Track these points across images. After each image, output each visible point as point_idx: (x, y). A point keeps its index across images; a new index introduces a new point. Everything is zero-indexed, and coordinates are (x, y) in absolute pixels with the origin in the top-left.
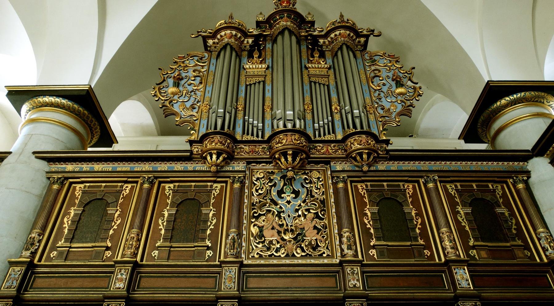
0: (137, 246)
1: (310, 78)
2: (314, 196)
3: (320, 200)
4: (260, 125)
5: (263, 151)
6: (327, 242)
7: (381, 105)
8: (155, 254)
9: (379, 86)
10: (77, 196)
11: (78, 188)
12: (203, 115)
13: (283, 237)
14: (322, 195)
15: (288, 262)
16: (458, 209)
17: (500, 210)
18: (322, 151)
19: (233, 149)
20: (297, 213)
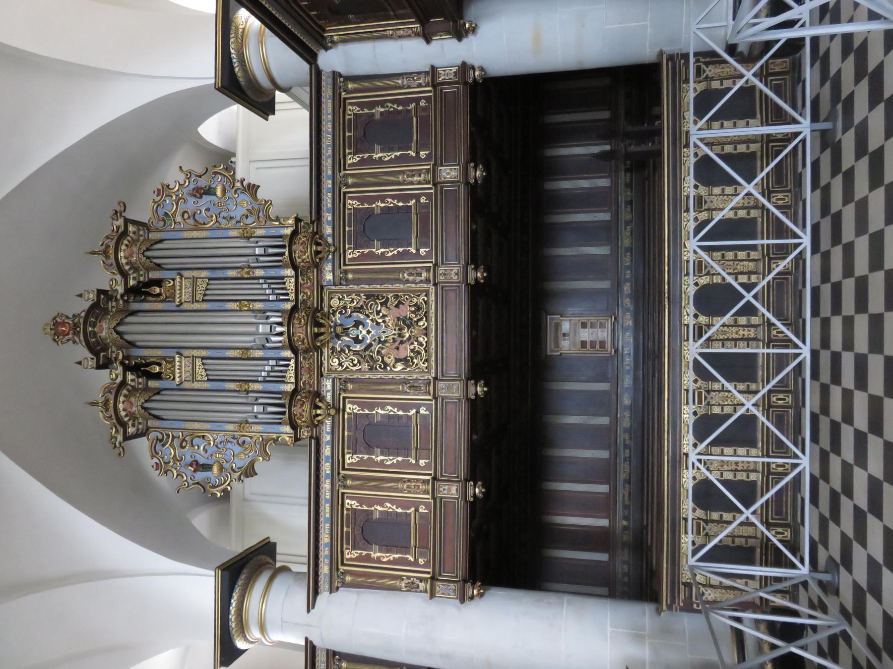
2: (362, 306)
3: (366, 299)
4: (272, 362)
5: (309, 359)
6: (412, 296)
9: (212, 216)
11: (348, 557)
15: (433, 334)
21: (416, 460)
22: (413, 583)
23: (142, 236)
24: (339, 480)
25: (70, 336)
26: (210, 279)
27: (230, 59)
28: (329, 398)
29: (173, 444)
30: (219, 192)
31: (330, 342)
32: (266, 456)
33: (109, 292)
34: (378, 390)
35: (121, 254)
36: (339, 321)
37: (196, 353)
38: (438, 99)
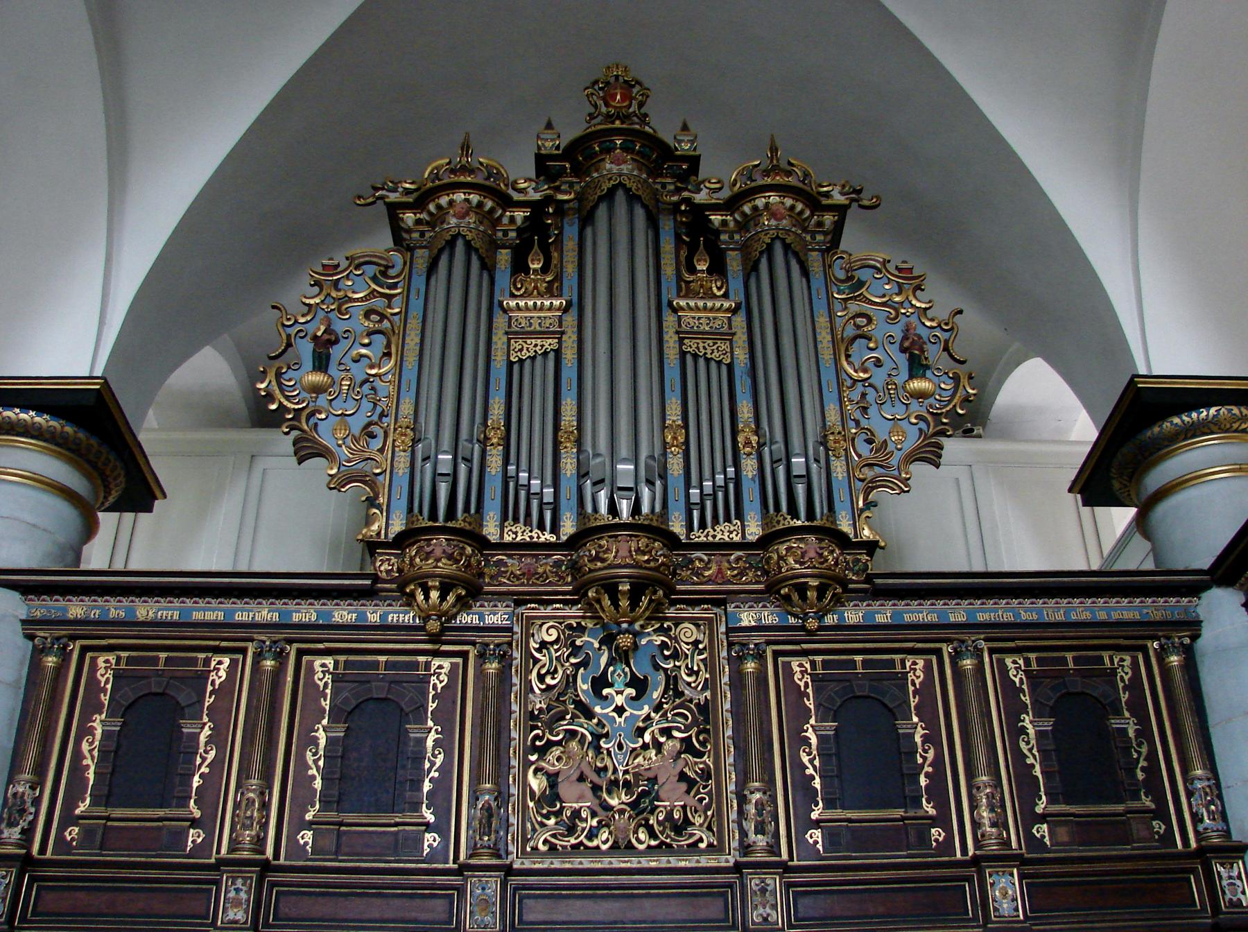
0: (264, 820)
1: (681, 340)
2: (682, 694)
3: (698, 705)
4: (549, 491)
6: (709, 813)
7: (867, 429)
8: (306, 840)
9: (865, 371)
10: (102, 685)
11: (101, 662)
12: (396, 459)
13: (605, 800)
14: (701, 690)
15: (617, 863)
16: (1023, 721)
17: (1118, 721)
18: (707, 573)
19: (480, 569)
20: (640, 740)
21: (311, 823)
22: (22, 811)
23: (813, 238)
24: (275, 642)
25: (604, 110)
26: (730, 367)
27: (1196, 407)
28: (466, 619)
29: (375, 297)
30: (917, 385)
31: (596, 621)
32: (338, 484)
33: (695, 178)
34: (482, 732)
35: (774, 198)
36: (644, 642)
37: (570, 340)
38: (1173, 865)
